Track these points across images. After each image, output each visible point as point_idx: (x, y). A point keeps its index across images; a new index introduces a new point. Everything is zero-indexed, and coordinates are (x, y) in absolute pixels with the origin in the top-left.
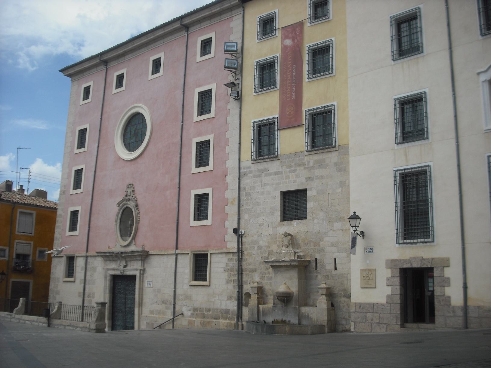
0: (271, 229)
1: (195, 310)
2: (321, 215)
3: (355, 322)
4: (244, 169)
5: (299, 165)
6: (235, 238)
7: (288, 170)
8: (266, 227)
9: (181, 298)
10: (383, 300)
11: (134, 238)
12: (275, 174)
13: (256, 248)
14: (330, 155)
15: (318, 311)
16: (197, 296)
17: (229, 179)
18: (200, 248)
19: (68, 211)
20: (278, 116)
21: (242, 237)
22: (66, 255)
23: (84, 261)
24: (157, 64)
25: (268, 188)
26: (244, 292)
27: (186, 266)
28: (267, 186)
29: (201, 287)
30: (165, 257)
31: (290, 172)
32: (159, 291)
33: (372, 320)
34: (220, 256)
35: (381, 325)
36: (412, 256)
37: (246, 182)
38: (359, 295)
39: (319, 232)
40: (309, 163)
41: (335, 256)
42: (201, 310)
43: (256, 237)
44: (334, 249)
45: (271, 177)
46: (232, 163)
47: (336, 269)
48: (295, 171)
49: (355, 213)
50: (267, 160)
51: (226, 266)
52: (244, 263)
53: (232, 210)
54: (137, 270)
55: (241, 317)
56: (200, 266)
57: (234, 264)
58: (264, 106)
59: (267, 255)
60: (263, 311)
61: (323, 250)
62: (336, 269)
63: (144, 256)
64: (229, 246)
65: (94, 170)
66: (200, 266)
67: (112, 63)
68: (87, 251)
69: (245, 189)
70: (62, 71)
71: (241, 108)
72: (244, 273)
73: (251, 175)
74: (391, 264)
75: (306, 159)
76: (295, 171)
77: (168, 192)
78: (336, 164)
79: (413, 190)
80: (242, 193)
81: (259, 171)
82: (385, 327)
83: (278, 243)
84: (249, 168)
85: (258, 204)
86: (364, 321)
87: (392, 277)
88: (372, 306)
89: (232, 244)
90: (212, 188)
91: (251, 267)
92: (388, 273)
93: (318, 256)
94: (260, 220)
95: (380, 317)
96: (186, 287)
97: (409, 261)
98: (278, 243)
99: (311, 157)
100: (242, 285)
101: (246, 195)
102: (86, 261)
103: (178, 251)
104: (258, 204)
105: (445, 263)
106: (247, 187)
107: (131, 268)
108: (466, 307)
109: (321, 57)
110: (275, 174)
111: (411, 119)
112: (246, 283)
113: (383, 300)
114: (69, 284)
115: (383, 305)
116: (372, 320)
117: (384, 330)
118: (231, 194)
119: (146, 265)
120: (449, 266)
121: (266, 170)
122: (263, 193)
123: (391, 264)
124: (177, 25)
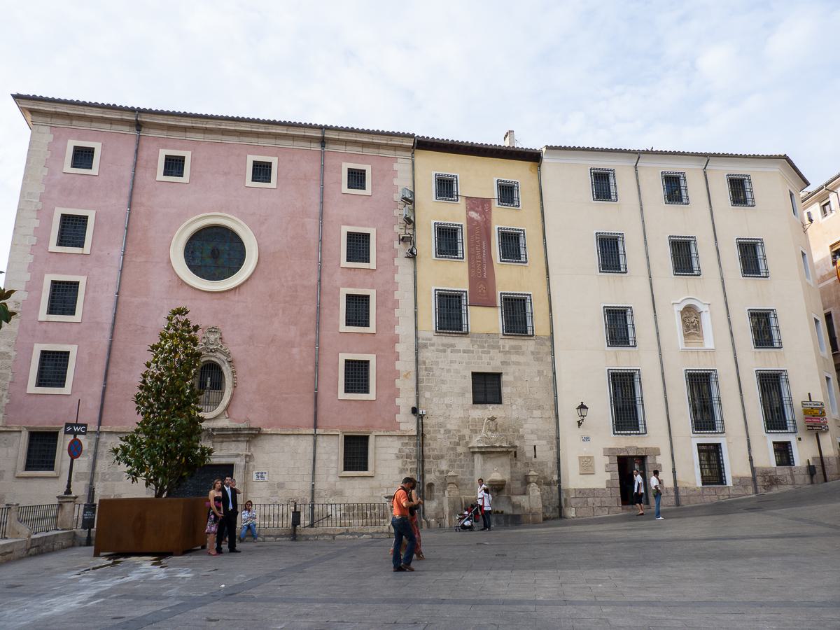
0: (462, 411)
1: (349, 508)
2: (520, 401)
3: (575, 508)
4: (423, 339)
5: (493, 347)
6: (414, 419)
7: (480, 350)
8: (452, 407)
9: (323, 493)
10: (603, 486)
11: (227, 409)
12: (465, 352)
13: (442, 431)
14: (526, 343)
15: (533, 500)
16: (358, 490)
17: (399, 348)
18: (356, 429)
19: (32, 349)
20: (467, 289)
21: (422, 418)
22: (27, 428)
23: (311, 443)
24: (262, 171)
25: (455, 366)
26: (427, 482)
27: (332, 451)
28: (455, 364)
29: (359, 478)
30: (292, 438)
31: (483, 352)
32: (281, 486)
33: (594, 504)
34: (390, 439)
35: (603, 508)
36: (627, 445)
37: (426, 355)
38: (574, 480)
39: (518, 418)
40: (504, 346)
41: (535, 443)
42: (360, 507)
43: (441, 419)
44: (534, 437)
45: (459, 354)
46: (404, 329)
47: (535, 457)
48: (489, 353)
49: (582, 403)
50: (454, 335)
51: (400, 452)
52: (426, 449)
53: (406, 386)
54: (238, 455)
55: (423, 513)
56: (356, 453)
57: (411, 449)
58: (454, 275)
59: (457, 440)
60: (465, 502)
61: (522, 437)
62: (535, 457)
63: (253, 435)
64: (402, 427)
65: (113, 289)
66: (356, 453)
67: (152, 131)
68: (100, 424)
69: (424, 363)
70: (17, 97)
71: (415, 268)
72: (426, 460)
73: (433, 348)
74: (609, 452)
75: (501, 342)
76: (489, 353)
77: (295, 351)
78: (533, 353)
79: (624, 387)
80: (422, 367)
81: (443, 345)
82: (607, 510)
83: (470, 427)
84: (430, 340)
85: (443, 382)
86: (586, 505)
87: (610, 463)
88: (594, 492)
89: (409, 425)
90: (375, 356)
91: (436, 453)
92: (607, 460)
93: (517, 443)
94: (447, 400)
95: (601, 501)
96: (332, 479)
97: (626, 449)
98: (470, 427)
99: (507, 341)
100: (423, 475)
101: (426, 369)
102: (98, 440)
103: (92, 428)
104: (443, 382)
105: (657, 452)
106: (427, 361)
107: (223, 453)
108: (676, 489)
109: (512, 245)
110: (465, 352)
111: (618, 326)
112: (429, 472)
113: (603, 486)
114: (36, 483)
115: (604, 489)
116: (594, 504)
117: (607, 513)
118: (405, 364)
119: (252, 449)
120: (659, 455)
121: (452, 346)
122: (449, 371)
123: (609, 452)
124: (318, 134)
